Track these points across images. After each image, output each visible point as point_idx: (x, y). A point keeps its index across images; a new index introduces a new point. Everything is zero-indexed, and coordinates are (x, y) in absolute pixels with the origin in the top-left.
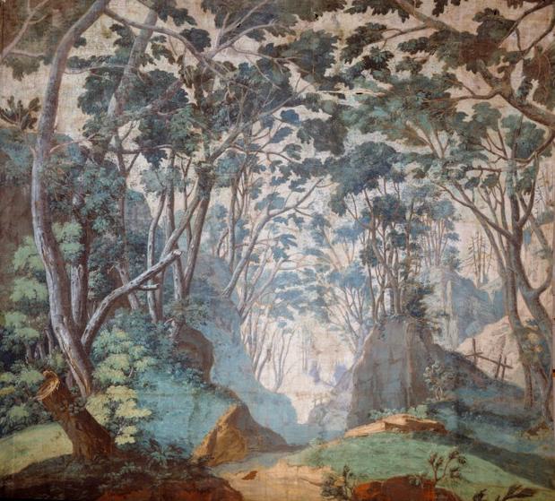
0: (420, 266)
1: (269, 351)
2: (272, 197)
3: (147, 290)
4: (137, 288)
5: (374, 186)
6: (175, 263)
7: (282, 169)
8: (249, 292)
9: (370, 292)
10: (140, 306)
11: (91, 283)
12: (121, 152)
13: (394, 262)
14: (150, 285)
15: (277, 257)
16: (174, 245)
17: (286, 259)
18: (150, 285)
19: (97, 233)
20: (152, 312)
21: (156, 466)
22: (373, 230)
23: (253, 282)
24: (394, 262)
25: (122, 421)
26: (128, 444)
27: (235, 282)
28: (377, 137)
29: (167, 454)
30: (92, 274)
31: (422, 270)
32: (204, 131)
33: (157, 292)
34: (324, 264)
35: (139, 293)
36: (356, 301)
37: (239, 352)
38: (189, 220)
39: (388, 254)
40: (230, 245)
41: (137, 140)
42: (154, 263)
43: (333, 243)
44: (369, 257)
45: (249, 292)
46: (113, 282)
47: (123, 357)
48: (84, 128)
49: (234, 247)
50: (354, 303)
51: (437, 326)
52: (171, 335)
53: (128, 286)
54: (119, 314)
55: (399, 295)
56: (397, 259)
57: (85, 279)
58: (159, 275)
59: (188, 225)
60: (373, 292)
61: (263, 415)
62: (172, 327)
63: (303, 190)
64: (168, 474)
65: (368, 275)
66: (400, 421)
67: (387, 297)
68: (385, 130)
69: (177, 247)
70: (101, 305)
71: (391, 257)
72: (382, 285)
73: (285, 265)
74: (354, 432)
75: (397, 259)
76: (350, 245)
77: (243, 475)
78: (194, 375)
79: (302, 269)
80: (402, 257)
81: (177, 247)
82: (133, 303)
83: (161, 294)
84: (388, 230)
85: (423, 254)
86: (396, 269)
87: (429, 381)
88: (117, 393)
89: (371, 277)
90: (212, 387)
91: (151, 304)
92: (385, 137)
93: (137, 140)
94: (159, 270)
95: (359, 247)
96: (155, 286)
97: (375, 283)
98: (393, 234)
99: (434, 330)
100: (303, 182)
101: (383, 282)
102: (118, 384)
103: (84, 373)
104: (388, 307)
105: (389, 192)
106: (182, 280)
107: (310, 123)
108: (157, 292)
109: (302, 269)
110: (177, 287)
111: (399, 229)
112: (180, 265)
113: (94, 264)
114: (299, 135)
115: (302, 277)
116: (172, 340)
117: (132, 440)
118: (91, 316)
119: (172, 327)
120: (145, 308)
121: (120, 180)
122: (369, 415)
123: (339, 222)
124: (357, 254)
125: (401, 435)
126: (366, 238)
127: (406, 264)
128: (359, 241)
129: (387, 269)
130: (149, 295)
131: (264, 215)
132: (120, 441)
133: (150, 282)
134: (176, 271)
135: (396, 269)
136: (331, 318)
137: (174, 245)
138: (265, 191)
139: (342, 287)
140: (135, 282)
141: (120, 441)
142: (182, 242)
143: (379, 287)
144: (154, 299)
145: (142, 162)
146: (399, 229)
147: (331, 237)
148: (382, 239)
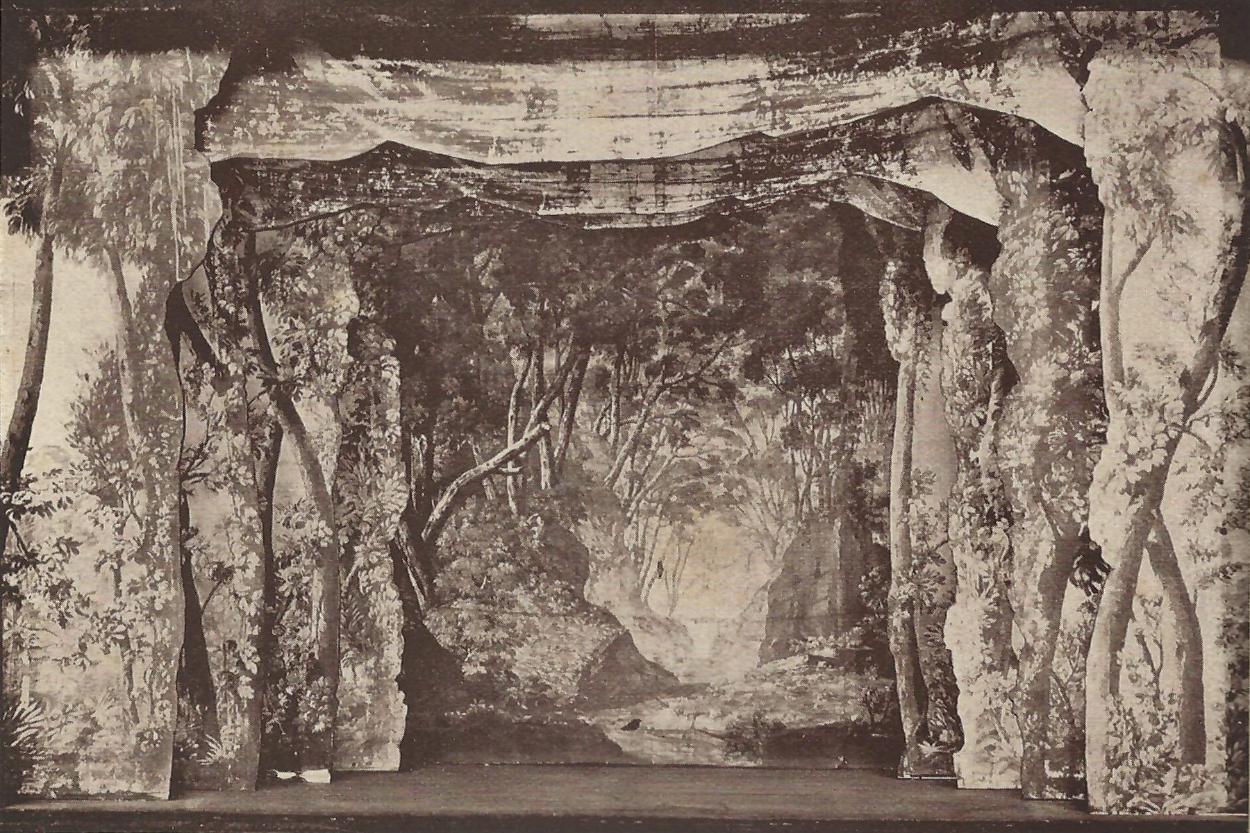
0: (858, 441)
1: (660, 564)
2: (668, 360)
3: (508, 474)
4: (496, 470)
5: (801, 342)
6: (543, 440)
7: (682, 324)
8: (636, 485)
9: (792, 482)
10: (497, 494)
11: (437, 460)
12: (478, 290)
13: (824, 441)
14: (510, 468)
15: (673, 442)
16: (542, 417)
17: (686, 443)
18: (510, 468)
19: (443, 395)
20: (512, 505)
21: (512, 705)
22: (798, 402)
23: (641, 471)
24: (824, 441)
25: (470, 643)
26: (479, 674)
27: (620, 469)
28: (808, 277)
29: (527, 690)
30: (438, 449)
31: (860, 446)
32: (582, 268)
33: (520, 477)
34: (734, 448)
35: (497, 478)
36: (776, 496)
37: (622, 562)
38: (562, 384)
39: (817, 432)
40: (614, 420)
41: (495, 274)
42: (516, 439)
43: (747, 420)
44: (793, 437)
45: (636, 485)
46: (462, 461)
47: (475, 561)
48: (387, 668)
49: (618, 424)
50: (772, 498)
51: (877, 520)
52: (536, 536)
53: (484, 467)
54: (471, 504)
55: (830, 485)
56: (829, 437)
57: (429, 457)
58: (522, 455)
59: (559, 392)
60: (797, 481)
61: (647, 646)
62: (537, 525)
63: (709, 351)
64: (527, 717)
65: (790, 462)
66: (829, 652)
67: (814, 488)
68: (816, 266)
69: (546, 420)
70: (449, 490)
71: (821, 436)
72: (809, 474)
73: (681, 451)
74: (768, 667)
75: (829, 437)
76: (769, 421)
77: (622, 724)
78: (564, 589)
79: (705, 456)
80: (835, 434)
81: (546, 420)
82: (489, 493)
83: (524, 479)
84: (818, 400)
85: (862, 425)
86: (828, 449)
87: (864, 594)
88: (465, 608)
89: (794, 463)
90: (585, 606)
91: (511, 493)
92: (818, 275)
93: (495, 274)
94: (522, 449)
95: (780, 423)
96: (517, 470)
97: (799, 471)
98: (823, 405)
99: (873, 524)
100: (710, 340)
101: (810, 470)
102: (467, 596)
103: (423, 578)
104: (815, 503)
105: (819, 349)
106: (551, 464)
107: (720, 259)
108: (520, 477)
109: (705, 456)
110: (545, 473)
111: (832, 398)
112: (548, 444)
113: (441, 436)
114: (704, 278)
115: (704, 466)
116: (537, 542)
117: (483, 670)
118: (436, 503)
119: (537, 525)
120: (503, 498)
121: (476, 326)
122: (788, 645)
123: (751, 391)
124: (778, 433)
125: (830, 670)
126: (790, 412)
127: (840, 442)
128: (780, 417)
129: (815, 452)
130: (510, 479)
131: (657, 382)
132: (469, 670)
133: (510, 464)
134: (543, 451)
135: (828, 449)
136: (744, 521)
137: (542, 417)
138: (661, 353)
139: (758, 477)
140: (491, 463)
141: (469, 670)
142: (554, 414)
143: (805, 477)
144: (516, 487)
145: (504, 303)
146: (832, 398)
147: (745, 412)
148: (809, 412)
